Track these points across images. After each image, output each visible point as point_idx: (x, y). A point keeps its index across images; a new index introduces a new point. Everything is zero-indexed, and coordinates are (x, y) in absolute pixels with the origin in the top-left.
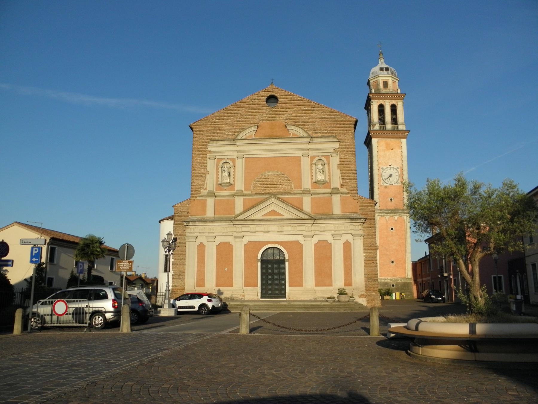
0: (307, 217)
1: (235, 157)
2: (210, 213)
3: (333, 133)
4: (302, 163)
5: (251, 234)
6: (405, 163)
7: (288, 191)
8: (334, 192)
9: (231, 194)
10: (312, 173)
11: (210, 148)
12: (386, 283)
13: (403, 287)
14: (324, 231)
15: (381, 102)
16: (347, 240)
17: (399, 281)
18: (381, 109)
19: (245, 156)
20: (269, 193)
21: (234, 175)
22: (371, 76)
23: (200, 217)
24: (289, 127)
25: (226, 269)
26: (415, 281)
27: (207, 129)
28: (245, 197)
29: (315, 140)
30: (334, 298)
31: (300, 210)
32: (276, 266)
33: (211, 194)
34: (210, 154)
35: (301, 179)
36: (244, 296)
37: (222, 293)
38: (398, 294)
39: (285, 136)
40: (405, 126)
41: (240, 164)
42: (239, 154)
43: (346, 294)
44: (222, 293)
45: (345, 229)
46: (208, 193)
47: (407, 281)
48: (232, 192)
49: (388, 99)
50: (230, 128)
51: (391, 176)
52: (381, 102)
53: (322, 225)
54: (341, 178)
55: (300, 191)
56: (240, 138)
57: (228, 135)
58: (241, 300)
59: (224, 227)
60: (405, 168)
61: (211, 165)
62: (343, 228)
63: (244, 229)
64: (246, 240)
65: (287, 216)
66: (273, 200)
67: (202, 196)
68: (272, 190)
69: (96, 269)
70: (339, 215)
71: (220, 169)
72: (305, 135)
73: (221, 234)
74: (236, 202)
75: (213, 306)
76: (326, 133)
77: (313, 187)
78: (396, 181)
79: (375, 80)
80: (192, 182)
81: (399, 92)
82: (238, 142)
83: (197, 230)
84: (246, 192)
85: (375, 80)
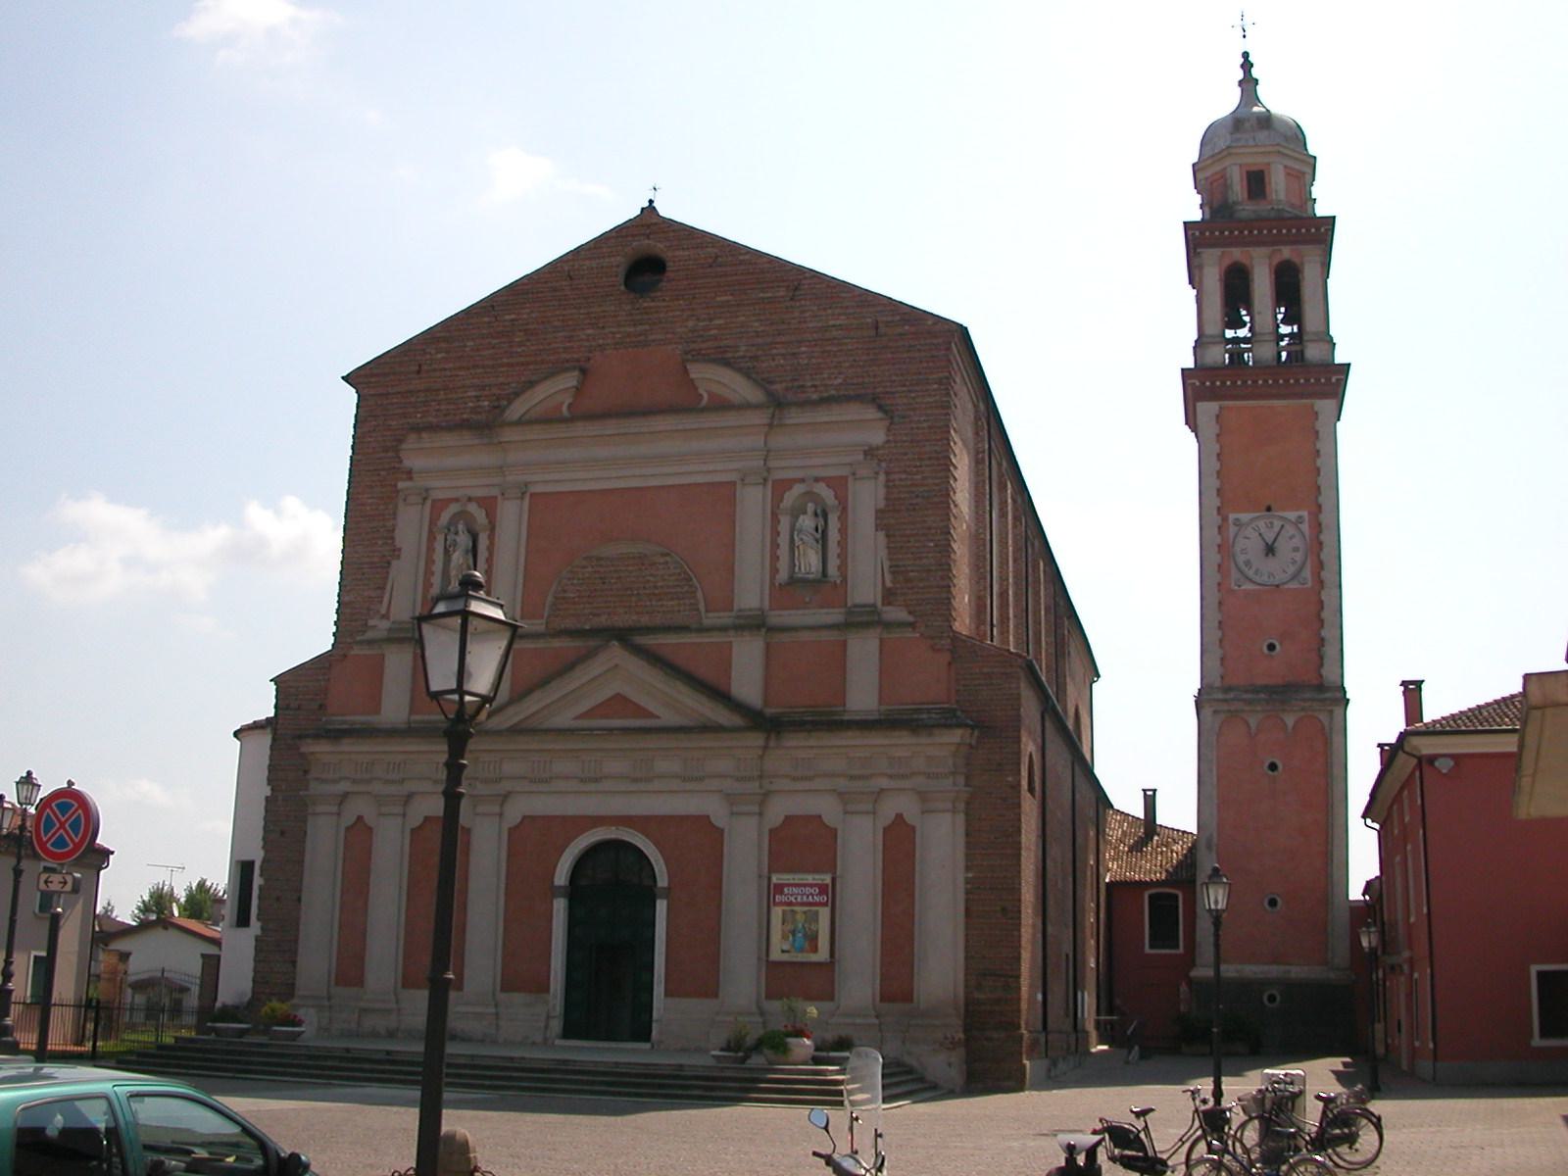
0: (737, 720)
8: (861, 619)
14: (811, 781)
33: (755, 624)
34: (408, 484)
41: (512, 519)
55: (725, 618)
67: (370, 642)
68: (623, 619)
71: (440, 538)
78: (1291, 570)
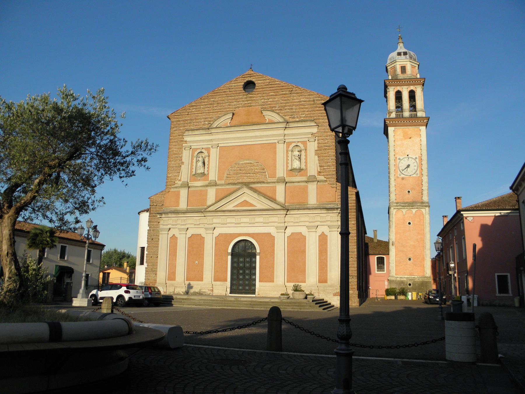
1: (210, 146)
2: (183, 205)
3: (311, 117)
4: (277, 150)
5: (222, 226)
6: (424, 153)
7: (261, 180)
8: (311, 180)
9: (204, 184)
10: (287, 160)
11: (186, 139)
12: (402, 282)
13: (419, 286)
14: (299, 223)
15: (399, 88)
16: (323, 232)
17: (417, 280)
18: (399, 96)
19: (220, 145)
20: (242, 183)
21: (208, 165)
22: (389, 61)
23: (173, 208)
24: (265, 113)
25: (197, 262)
26: (435, 280)
27: (184, 119)
28: (217, 187)
29: (292, 125)
30: (288, 295)
31: (273, 200)
32: (248, 260)
34: (186, 145)
35: (275, 167)
36: (212, 290)
37: (192, 288)
38: (415, 294)
39: (261, 123)
40: (424, 113)
41: (214, 153)
42: (214, 143)
43: (301, 291)
44: (192, 288)
45: (322, 220)
46: (181, 184)
47: (425, 280)
48: (206, 183)
49: (406, 85)
50: (207, 117)
51: (408, 166)
52: (399, 88)
53: (294, 216)
54: (318, 165)
55: (274, 180)
56: (215, 126)
57: (204, 125)
58: (209, 295)
59: (192, 220)
60: (425, 157)
61: (186, 155)
62: (319, 219)
63: (215, 221)
64: (217, 232)
65: (259, 206)
66: (245, 190)
67: (176, 187)
69: (67, 260)
70: (315, 204)
72: (281, 120)
73: (192, 226)
74: (208, 193)
75: (130, 298)
76: (304, 117)
77: (288, 176)
78: (414, 171)
79: (393, 65)
80: (168, 173)
81: (418, 76)
82: (213, 131)
83: (170, 222)
84: (219, 182)
85: (393, 65)
